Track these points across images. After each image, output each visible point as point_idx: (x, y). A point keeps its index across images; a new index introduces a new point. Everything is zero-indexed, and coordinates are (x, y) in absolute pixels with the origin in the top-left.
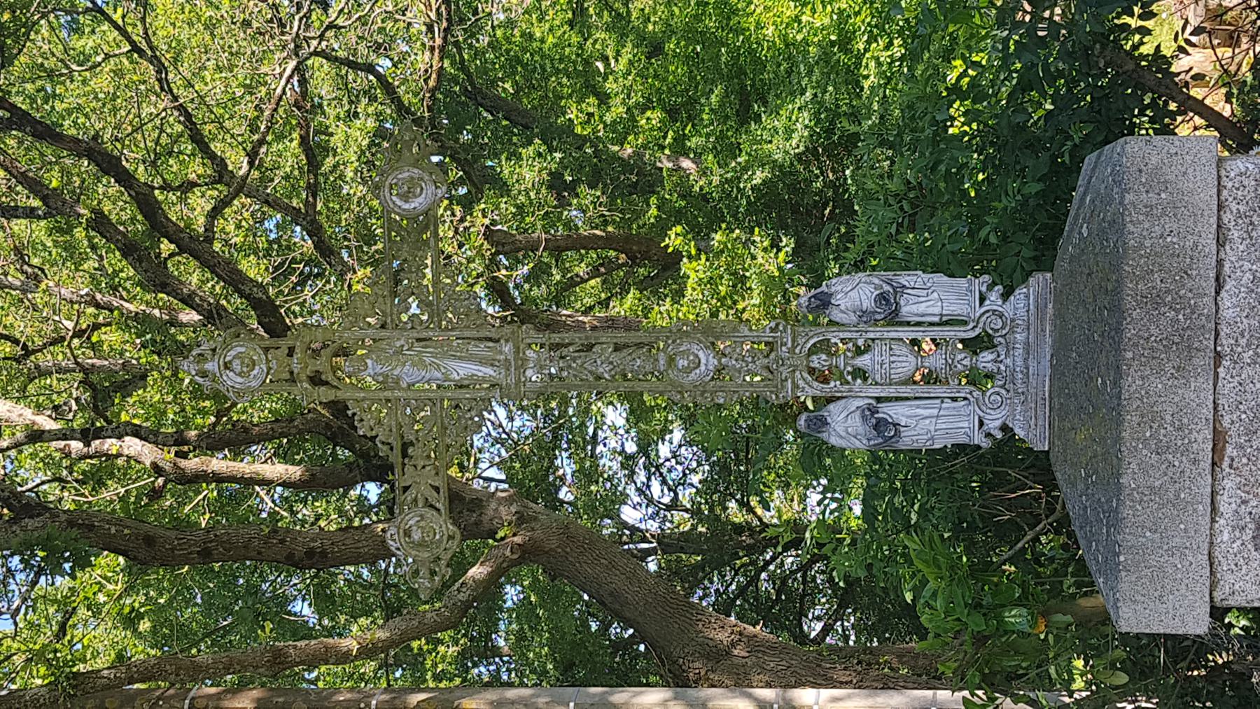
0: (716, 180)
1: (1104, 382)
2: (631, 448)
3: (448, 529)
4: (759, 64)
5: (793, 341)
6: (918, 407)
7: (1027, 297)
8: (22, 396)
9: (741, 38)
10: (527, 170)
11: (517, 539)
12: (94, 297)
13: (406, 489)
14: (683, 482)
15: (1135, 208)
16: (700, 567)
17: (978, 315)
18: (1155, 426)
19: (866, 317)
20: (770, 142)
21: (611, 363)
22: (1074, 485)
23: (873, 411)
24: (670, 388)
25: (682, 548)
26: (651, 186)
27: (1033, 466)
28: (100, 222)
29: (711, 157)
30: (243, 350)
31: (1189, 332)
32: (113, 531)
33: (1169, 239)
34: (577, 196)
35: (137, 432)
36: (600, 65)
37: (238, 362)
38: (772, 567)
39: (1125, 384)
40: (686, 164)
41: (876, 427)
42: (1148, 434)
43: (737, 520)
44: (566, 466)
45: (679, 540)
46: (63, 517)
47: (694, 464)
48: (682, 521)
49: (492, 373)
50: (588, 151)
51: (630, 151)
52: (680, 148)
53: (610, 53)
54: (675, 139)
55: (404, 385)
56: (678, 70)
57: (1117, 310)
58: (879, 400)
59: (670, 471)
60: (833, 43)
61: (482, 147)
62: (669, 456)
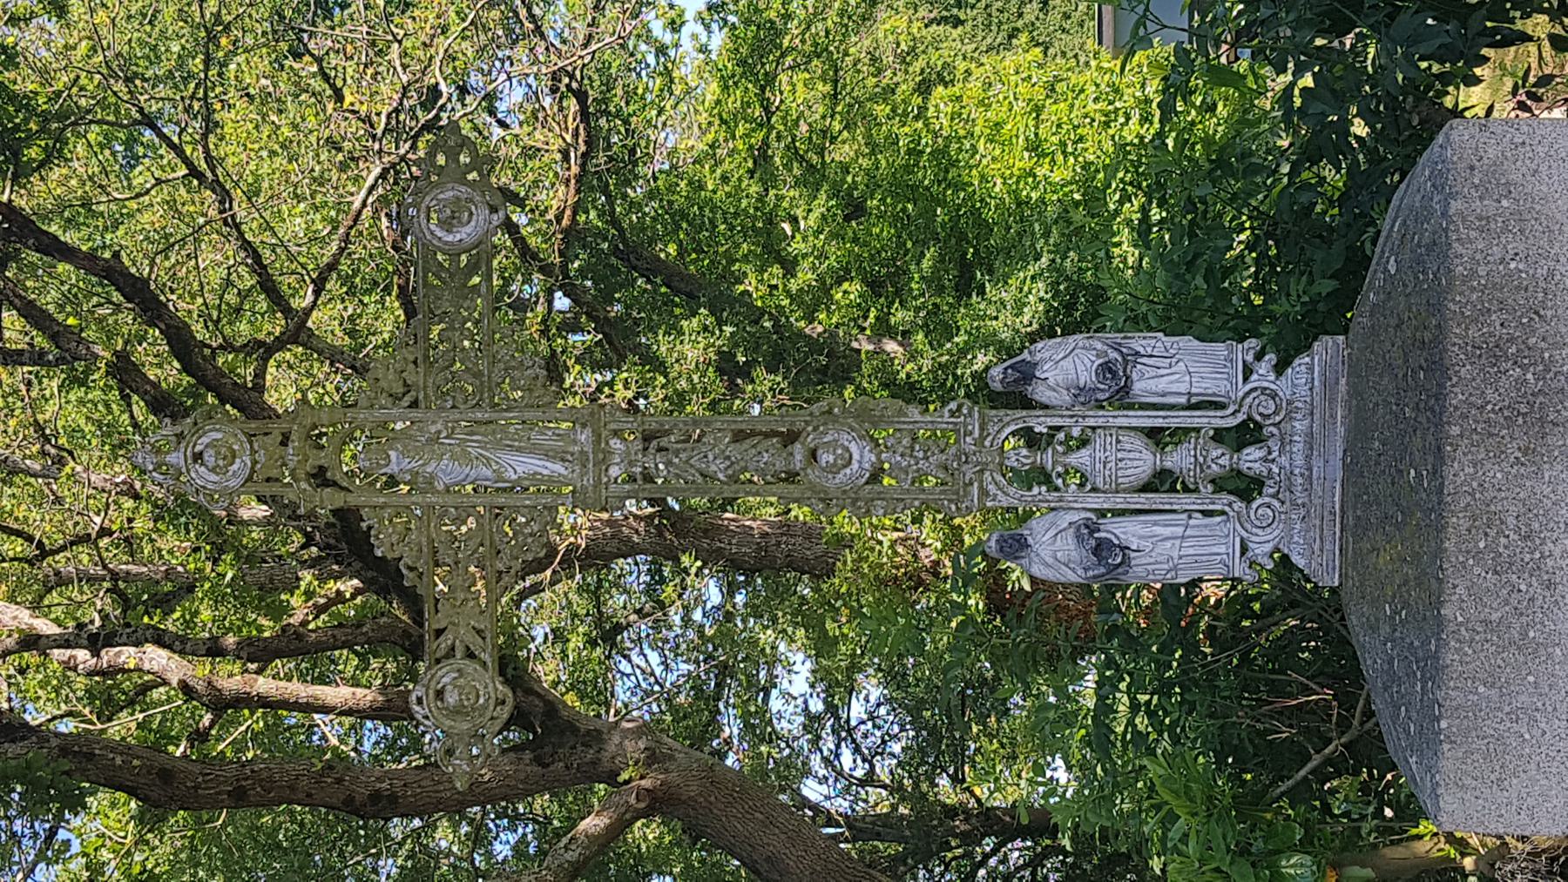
0: (927, 364)
1: (1419, 475)
2: (817, 706)
3: (496, 689)
4: (985, 228)
5: (982, 429)
6: (1155, 524)
7: (1311, 369)
8: (36, 606)
9: (962, 195)
10: (690, 347)
11: (646, 783)
12: (132, 486)
13: (439, 633)
14: (880, 750)
15: (1464, 220)
16: (899, 859)
17: (1241, 394)
18: (1492, 533)
19: (1083, 395)
20: (996, 318)
21: (728, 458)
22: (1374, 629)
23: (1092, 528)
24: (808, 494)
25: (878, 834)
26: (849, 371)
27: (1322, 673)
28: (125, 373)
29: (920, 336)
30: (219, 436)
31: (1541, 399)
32: (118, 761)
33: (1513, 265)
34: (753, 381)
35: (160, 639)
36: (787, 227)
37: (211, 452)
38: (992, 862)
39: (1449, 472)
40: (891, 346)
41: (1097, 551)
42: (1482, 545)
43: (948, 801)
44: (731, 727)
45: (873, 823)
46: (54, 742)
47: (896, 728)
48: (878, 800)
49: (562, 471)
50: (767, 324)
51: (820, 329)
52: (884, 328)
53: (799, 213)
54: (877, 318)
55: (441, 487)
56: (883, 231)
57: (1438, 368)
58: (1102, 513)
59: (865, 736)
60: (1077, 204)
61: (636, 322)
62: (865, 717)
